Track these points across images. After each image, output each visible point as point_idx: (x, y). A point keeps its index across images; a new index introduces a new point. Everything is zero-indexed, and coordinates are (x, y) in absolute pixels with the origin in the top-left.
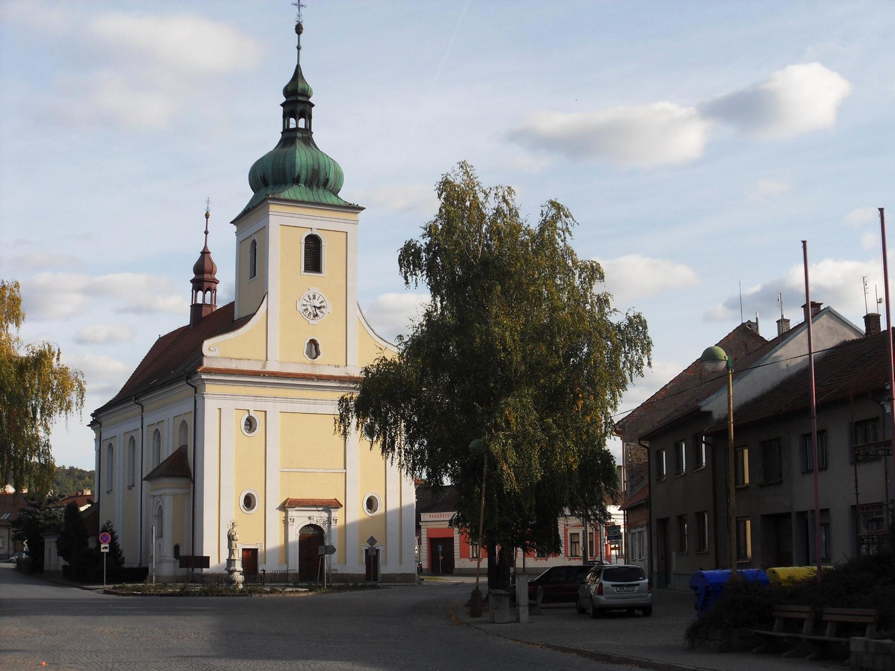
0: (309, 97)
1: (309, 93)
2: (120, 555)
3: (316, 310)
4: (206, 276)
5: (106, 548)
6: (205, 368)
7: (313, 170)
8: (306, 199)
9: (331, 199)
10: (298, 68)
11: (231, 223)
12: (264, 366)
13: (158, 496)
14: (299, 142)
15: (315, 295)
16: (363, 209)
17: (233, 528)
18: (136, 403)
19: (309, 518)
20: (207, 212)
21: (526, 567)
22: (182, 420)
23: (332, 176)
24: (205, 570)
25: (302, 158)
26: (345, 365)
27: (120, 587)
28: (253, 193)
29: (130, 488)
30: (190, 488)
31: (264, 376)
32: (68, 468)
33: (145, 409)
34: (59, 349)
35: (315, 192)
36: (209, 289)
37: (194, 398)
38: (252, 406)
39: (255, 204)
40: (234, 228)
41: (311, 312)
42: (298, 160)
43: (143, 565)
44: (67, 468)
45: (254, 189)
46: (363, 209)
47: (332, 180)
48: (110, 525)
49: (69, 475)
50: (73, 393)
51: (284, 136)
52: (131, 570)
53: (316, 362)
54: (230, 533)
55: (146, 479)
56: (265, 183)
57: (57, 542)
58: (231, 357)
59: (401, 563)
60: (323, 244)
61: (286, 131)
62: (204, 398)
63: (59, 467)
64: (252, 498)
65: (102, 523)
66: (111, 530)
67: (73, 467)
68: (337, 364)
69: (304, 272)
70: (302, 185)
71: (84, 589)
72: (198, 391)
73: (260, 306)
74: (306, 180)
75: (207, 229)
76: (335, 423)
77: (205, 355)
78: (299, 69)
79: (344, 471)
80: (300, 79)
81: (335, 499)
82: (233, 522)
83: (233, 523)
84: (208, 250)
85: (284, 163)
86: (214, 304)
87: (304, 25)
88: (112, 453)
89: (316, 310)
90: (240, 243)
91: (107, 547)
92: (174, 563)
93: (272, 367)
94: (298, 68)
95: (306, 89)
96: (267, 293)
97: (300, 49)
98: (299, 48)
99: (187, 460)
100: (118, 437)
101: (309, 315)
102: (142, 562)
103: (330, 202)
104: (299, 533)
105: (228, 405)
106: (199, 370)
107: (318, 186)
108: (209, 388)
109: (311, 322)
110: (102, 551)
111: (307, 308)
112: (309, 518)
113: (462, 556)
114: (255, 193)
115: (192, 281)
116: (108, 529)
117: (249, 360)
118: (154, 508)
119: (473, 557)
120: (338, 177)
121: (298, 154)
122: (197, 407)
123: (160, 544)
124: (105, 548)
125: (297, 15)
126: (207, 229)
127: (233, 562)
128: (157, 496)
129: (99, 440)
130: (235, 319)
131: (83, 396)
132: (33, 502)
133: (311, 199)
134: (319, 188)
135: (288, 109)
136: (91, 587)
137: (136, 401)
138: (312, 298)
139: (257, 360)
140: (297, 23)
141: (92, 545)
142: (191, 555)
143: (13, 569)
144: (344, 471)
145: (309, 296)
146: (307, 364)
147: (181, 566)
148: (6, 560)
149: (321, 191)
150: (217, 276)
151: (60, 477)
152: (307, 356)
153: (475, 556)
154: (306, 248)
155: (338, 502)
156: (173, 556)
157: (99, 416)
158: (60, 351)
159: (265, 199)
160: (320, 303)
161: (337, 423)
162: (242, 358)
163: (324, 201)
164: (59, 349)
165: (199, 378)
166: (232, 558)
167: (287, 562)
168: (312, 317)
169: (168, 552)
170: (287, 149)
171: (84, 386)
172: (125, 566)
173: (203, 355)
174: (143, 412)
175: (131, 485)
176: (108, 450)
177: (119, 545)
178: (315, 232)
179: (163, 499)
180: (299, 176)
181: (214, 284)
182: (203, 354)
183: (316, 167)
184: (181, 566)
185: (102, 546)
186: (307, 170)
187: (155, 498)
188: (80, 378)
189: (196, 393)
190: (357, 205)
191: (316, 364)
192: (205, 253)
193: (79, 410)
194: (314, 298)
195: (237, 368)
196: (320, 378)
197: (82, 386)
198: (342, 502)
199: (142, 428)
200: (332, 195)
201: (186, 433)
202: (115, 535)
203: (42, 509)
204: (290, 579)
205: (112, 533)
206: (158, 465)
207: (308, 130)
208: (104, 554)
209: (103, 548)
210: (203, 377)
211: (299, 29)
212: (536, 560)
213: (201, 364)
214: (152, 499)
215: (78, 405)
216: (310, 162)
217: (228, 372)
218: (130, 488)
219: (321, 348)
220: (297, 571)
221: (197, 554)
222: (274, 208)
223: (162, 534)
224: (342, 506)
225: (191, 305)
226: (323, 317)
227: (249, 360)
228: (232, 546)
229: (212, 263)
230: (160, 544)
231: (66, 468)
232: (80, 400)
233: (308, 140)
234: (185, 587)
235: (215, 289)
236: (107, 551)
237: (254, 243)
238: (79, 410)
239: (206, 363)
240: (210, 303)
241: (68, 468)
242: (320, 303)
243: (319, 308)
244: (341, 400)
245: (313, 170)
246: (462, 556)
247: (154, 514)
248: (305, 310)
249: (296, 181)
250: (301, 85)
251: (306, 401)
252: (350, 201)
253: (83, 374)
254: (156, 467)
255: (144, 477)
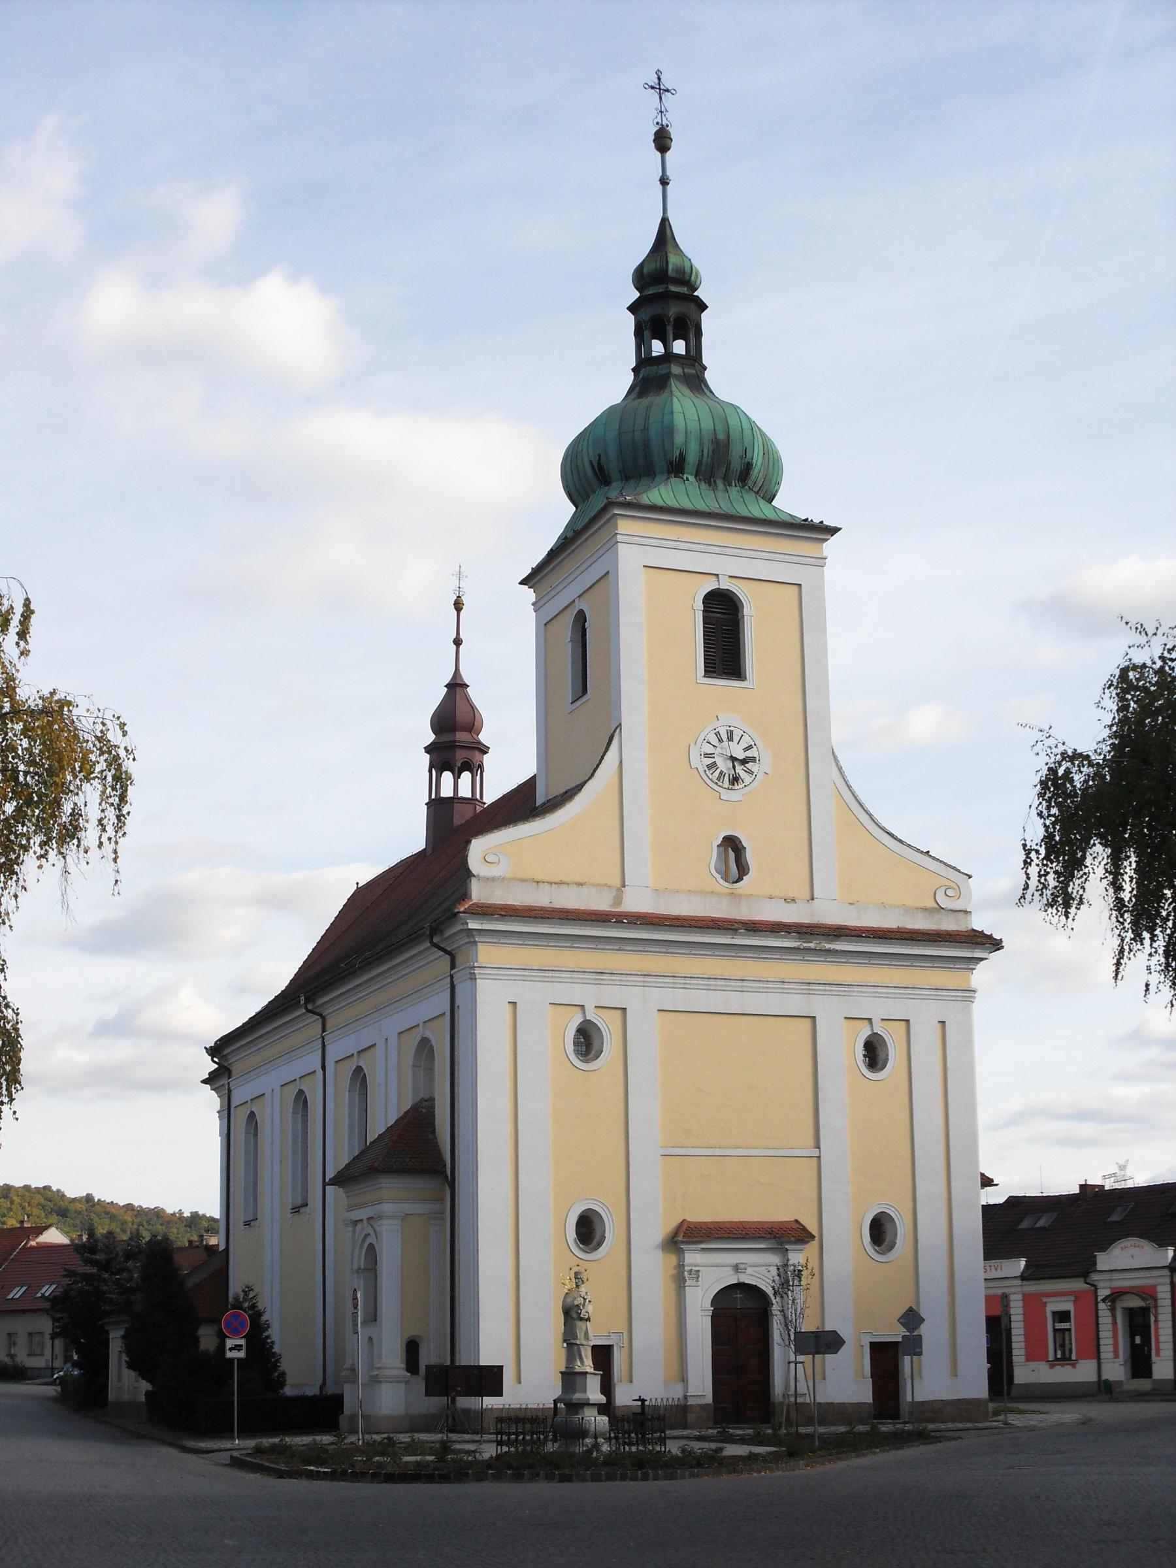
0: (696, 289)
1: (693, 278)
2: (275, 1366)
3: (734, 767)
4: (461, 736)
5: (237, 1348)
6: (477, 905)
7: (716, 442)
8: (701, 506)
9: (758, 509)
10: (664, 224)
11: (523, 582)
12: (618, 900)
13: (365, 1222)
14: (678, 383)
15: (732, 732)
16: (834, 531)
17: (577, 1286)
18: (308, 1011)
19: (737, 1268)
20: (459, 597)
21: (1104, 1377)
22: (419, 1038)
23: (758, 459)
24: (489, 1402)
25: (688, 415)
26: (808, 896)
27: (273, 1449)
28: (574, 509)
29: (296, 1210)
30: (442, 1200)
31: (619, 922)
32: (189, 1215)
33: (328, 1025)
34: (27, 599)
35: (720, 494)
36: (467, 766)
37: (448, 980)
38: (589, 995)
39: (579, 527)
40: (529, 594)
41: (725, 771)
42: (679, 420)
43: (330, 1390)
44: (187, 1214)
45: (576, 496)
46: (834, 531)
47: (759, 465)
48: (251, 1295)
49: (190, 1227)
50: (86, 787)
51: (641, 376)
52: (301, 1401)
53: (739, 891)
54: (569, 1300)
55: (336, 1181)
56: (602, 477)
57: (123, 1337)
58: (538, 877)
59: (954, 1373)
60: (746, 611)
61: (644, 362)
62: (473, 978)
63: (172, 1212)
64: (596, 1221)
65: (235, 1288)
66: (253, 1307)
67: (196, 1212)
68: (791, 895)
69: (704, 676)
70: (689, 477)
71: (185, 1450)
72: (458, 962)
73: (602, 758)
74: (707, 463)
75: (458, 633)
76: (1027, 863)
77: (475, 872)
78: (668, 228)
79: (815, 1153)
80: (670, 248)
81: (797, 1221)
82: (576, 1269)
83: (576, 1273)
84: (462, 680)
85: (645, 429)
86: (478, 797)
87: (673, 132)
88: (256, 1135)
89: (734, 767)
90: (545, 627)
91: (241, 1346)
92: (407, 1383)
93: (637, 902)
94: (664, 224)
95: (688, 270)
96: (620, 724)
97: (668, 184)
98: (664, 182)
99: (434, 1132)
100: (268, 1096)
101: (718, 779)
102: (328, 1381)
103: (757, 514)
104: (713, 1304)
105: (533, 994)
106: (462, 909)
107: (727, 481)
108: (487, 954)
109: (725, 794)
110: (229, 1355)
111: (715, 763)
112: (737, 1268)
113: (1030, 1357)
114: (576, 507)
115: (428, 750)
116: (246, 1305)
117: (581, 884)
118: (357, 1248)
119: (1057, 1359)
120: (771, 463)
121: (677, 406)
122: (458, 1002)
123: (370, 1339)
124: (235, 1348)
125: (657, 109)
126: (458, 633)
127: (579, 1378)
128: (362, 1220)
129: (227, 1112)
130: (537, 805)
131: (123, 798)
132: (93, 1256)
133: (713, 506)
134: (730, 485)
135: (647, 313)
136: (203, 1445)
137: (310, 1007)
138: (724, 737)
139: (599, 885)
140: (657, 128)
141: (207, 1340)
142: (448, 1363)
143: (51, 1399)
144: (815, 1153)
145: (717, 734)
146: (719, 894)
147: (429, 1393)
148: (45, 1380)
149: (734, 492)
150: (483, 737)
151: (175, 1231)
152: (718, 876)
153: (1059, 1356)
154: (706, 621)
155: (804, 1229)
156: (404, 1366)
157: (225, 1053)
158: (32, 607)
159: (604, 510)
160: (746, 749)
161: (1036, 861)
162: (564, 880)
163: (744, 512)
164: (27, 599)
165: (461, 927)
166: (578, 1368)
167: (683, 1379)
168: (726, 784)
169: (392, 1358)
170: (656, 400)
171: (128, 765)
172: (288, 1391)
173: (469, 874)
174: (324, 1030)
175: (299, 1203)
176: (247, 1128)
177: (272, 1343)
178: (725, 584)
179: (378, 1229)
180: (682, 458)
181: (477, 753)
182: (469, 871)
183: (721, 436)
184: (429, 1393)
185: (229, 1343)
186: (701, 444)
187: (359, 1227)
188: (114, 736)
189: (453, 967)
190: (822, 522)
191: (740, 896)
192: (456, 686)
193: (108, 848)
194: (730, 738)
195: (551, 905)
196: (754, 927)
197: (120, 765)
198: (813, 1228)
199: (324, 1068)
200: (762, 502)
201: (430, 1070)
202: (264, 1318)
203: (114, 1270)
204: (691, 1417)
205: (256, 1315)
206: (364, 1147)
207: (694, 357)
208: (233, 1363)
209: (231, 1349)
210: (473, 925)
211: (662, 141)
212: (1052, 1366)
213: (465, 895)
214: (350, 1229)
215: (104, 830)
216: (707, 424)
217: (532, 914)
218: (296, 1210)
219: (750, 857)
220: (709, 1399)
221: (464, 1360)
222: (627, 527)
223: (376, 1316)
224: (813, 1237)
225: (427, 801)
226: (754, 782)
227: (581, 884)
228: (576, 1338)
229: (472, 708)
230: (370, 1339)
231: (185, 1215)
232: (111, 814)
233: (697, 382)
234: (445, 1447)
235: (479, 765)
236: (241, 1354)
237: (581, 618)
238: (108, 848)
239: (478, 893)
240: (470, 796)
241: (189, 1215)
242: (746, 749)
243: (744, 762)
244: (1048, 779)
245: (716, 442)
246: (1030, 1357)
247: (355, 1267)
248: (710, 767)
249: (676, 468)
250: (673, 260)
251: (720, 983)
252: (801, 513)
253: (125, 724)
254: (356, 1153)
255: (327, 1181)
